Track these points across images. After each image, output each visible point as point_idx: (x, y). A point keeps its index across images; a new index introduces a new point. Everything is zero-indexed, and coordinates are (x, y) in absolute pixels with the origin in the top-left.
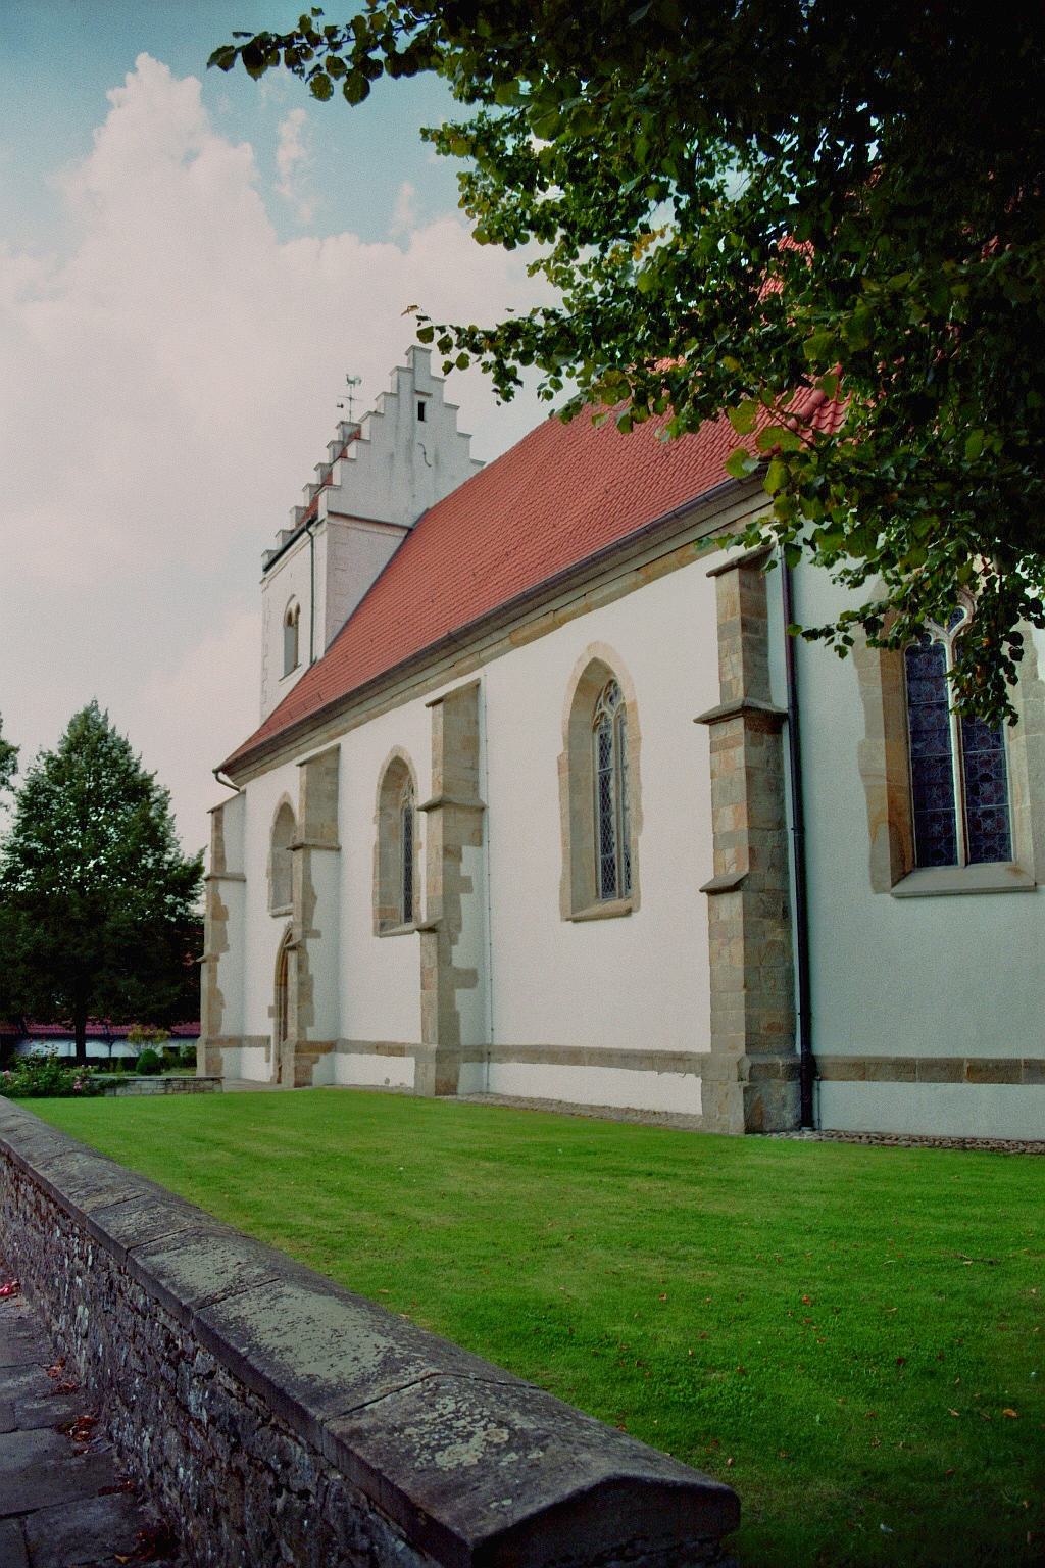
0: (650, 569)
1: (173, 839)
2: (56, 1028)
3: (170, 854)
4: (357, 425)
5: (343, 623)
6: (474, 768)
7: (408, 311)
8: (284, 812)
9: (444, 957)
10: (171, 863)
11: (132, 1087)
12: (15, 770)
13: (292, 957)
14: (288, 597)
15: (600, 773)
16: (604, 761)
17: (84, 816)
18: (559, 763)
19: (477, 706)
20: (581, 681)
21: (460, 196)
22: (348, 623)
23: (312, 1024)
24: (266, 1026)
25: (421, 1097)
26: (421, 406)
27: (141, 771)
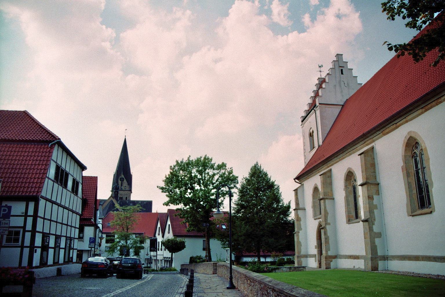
0: (427, 108)
1: (282, 199)
2: (252, 254)
3: (281, 203)
4: (323, 78)
5: (326, 134)
6: (375, 172)
7: (384, 44)
8: (316, 189)
9: (371, 229)
10: (281, 206)
11: (280, 270)
12: (238, 183)
13: (322, 231)
14: (310, 128)
15: (415, 170)
16: (417, 166)
17: (257, 194)
18: (402, 169)
19: (373, 154)
20: (407, 143)
21: (382, 9)
22: (328, 134)
23: (329, 250)
24: (314, 251)
25: (367, 272)
26: (342, 70)
27: (271, 181)
